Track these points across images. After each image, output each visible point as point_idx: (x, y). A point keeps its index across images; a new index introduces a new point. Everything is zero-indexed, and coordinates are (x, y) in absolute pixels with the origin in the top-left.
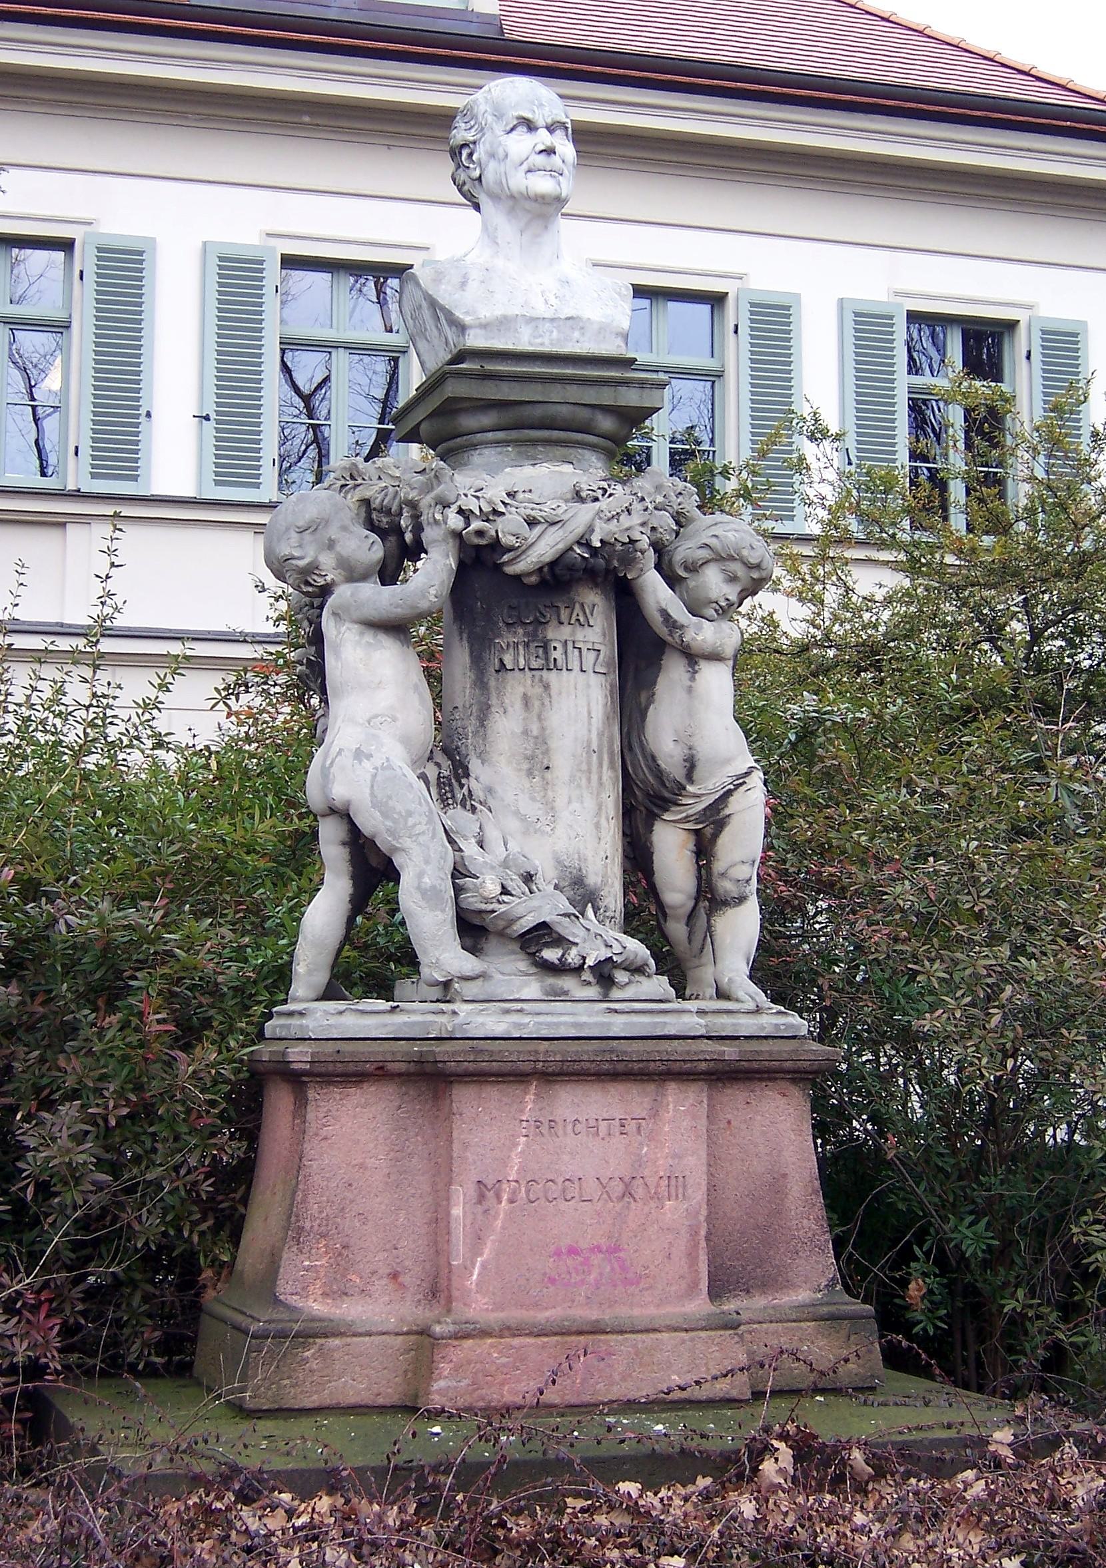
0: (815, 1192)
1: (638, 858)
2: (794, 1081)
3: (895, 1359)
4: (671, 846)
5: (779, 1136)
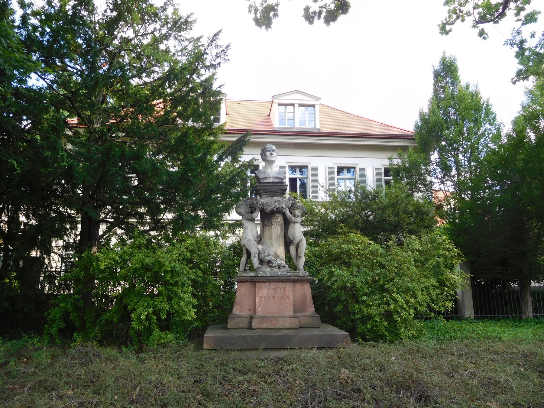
1: (287, 251)
3: (322, 322)
4: (292, 249)
5: (306, 290)
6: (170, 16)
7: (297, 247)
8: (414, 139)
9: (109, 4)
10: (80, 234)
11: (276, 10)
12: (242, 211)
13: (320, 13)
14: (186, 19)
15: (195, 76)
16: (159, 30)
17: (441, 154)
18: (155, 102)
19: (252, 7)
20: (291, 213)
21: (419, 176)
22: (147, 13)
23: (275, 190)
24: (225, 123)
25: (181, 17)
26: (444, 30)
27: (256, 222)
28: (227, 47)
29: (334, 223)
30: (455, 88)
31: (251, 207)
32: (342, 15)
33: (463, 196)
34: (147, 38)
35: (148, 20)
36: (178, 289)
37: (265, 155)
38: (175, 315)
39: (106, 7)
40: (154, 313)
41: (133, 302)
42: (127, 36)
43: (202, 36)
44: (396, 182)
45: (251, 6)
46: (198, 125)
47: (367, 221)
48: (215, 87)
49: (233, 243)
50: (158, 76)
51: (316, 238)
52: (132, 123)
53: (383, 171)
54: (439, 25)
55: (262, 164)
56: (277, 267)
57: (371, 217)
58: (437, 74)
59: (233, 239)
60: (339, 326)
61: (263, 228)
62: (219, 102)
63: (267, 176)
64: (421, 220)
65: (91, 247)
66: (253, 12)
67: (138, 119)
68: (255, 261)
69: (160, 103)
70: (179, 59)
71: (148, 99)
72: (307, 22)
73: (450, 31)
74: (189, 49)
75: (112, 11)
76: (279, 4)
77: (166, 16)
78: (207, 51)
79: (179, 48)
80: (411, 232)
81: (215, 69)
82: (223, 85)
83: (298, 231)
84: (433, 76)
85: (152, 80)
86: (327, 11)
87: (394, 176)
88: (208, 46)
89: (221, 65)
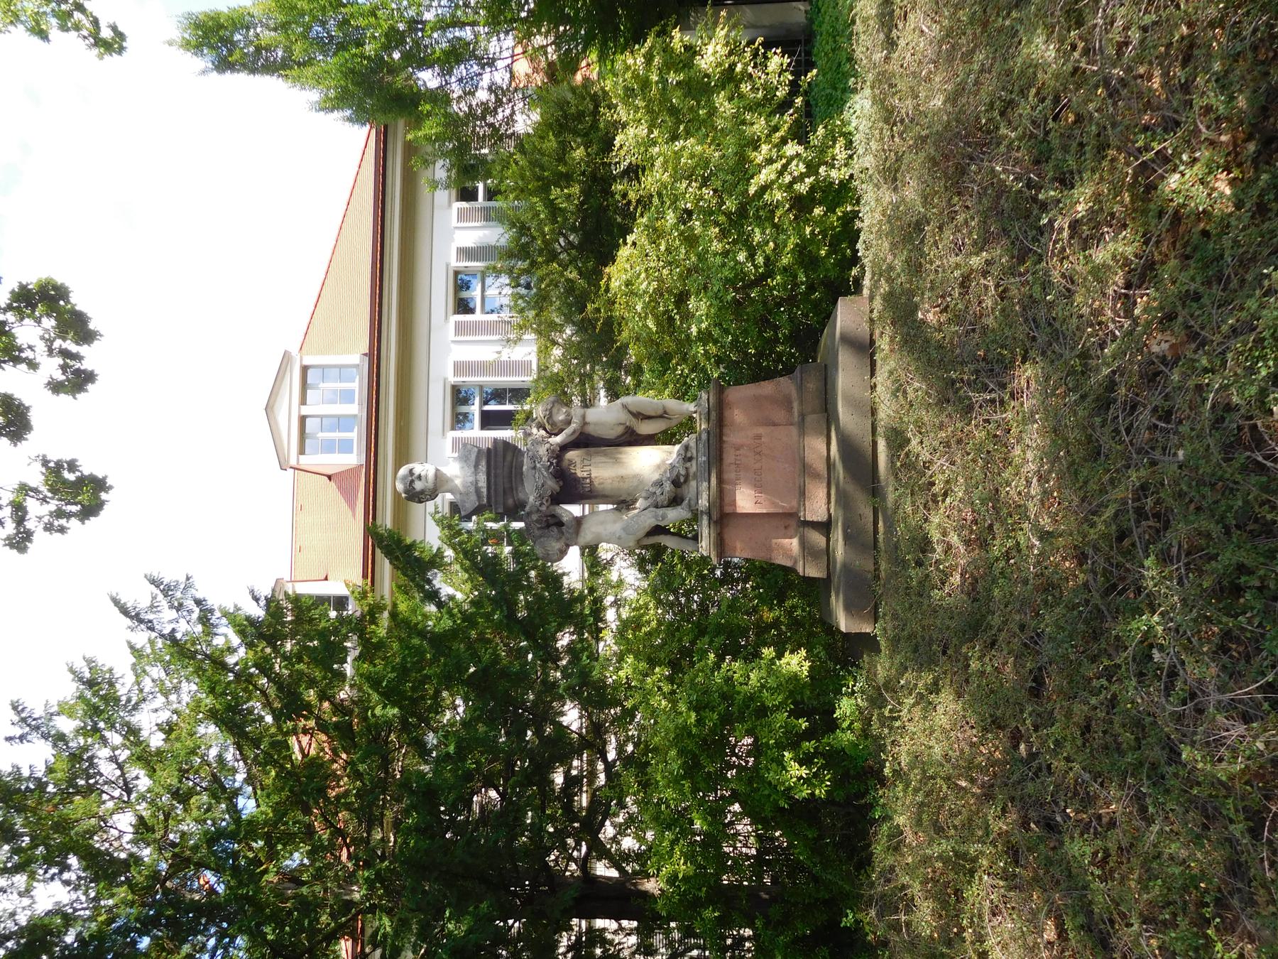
1: (650, 440)
4: (646, 428)
6: (77, 723)
8: (386, 127)
9: (48, 876)
10: (617, 919)
11: (59, 465)
12: (556, 545)
13: (65, 354)
14: (84, 683)
15: (231, 660)
16: (114, 749)
17: (424, 64)
18: (297, 756)
19: (52, 524)
20: (561, 431)
21: (476, 118)
22: (71, 782)
23: (506, 469)
24: (347, 585)
25: (81, 697)
26: (112, 44)
27: (587, 512)
28: (154, 582)
29: (584, 326)
30: (261, 22)
31: (548, 526)
32: (72, 300)
33: (523, 14)
34: (137, 778)
35: (89, 777)
36: (739, 693)
37: (422, 492)
38: (799, 698)
39: (57, 883)
40: (794, 746)
41: (769, 796)
42: (131, 830)
43: (129, 643)
44: (488, 175)
45: (49, 528)
46: (352, 646)
47: (580, 248)
48: (258, 612)
50: (231, 749)
51: (620, 368)
52: (347, 809)
53: (464, 204)
54: (101, 56)
56: (688, 464)
57: (571, 238)
58: (224, 65)
59: (624, 564)
61: (595, 497)
62: (296, 600)
63: (472, 489)
64: (578, 119)
65: (646, 895)
66: (63, 522)
67: (338, 797)
68: (674, 516)
69: (299, 742)
70: (186, 698)
71: (289, 776)
72: (90, 387)
73: (114, 28)
74: (163, 675)
75: (65, 867)
76: (44, 456)
77: (78, 732)
78: (166, 631)
79: (161, 700)
80: (608, 145)
81: (212, 611)
82: (252, 592)
83: (605, 413)
84: (228, 75)
85: (241, 763)
86: (60, 337)
87: (475, 178)
88: (152, 629)
89: (199, 596)
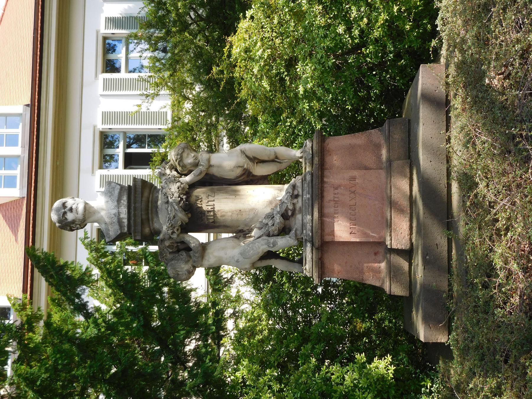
0: (354, 135)
2: (324, 142)
4: (260, 170)
7: (256, 160)
12: (185, 267)
20: (190, 172)
23: (144, 204)
29: (211, 85)
31: (178, 251)
37: (73, 222)
47: (207, 20)
49: (248, 283)
55: (91, 229)
56: (295, 201)
59: (242, 283)
60: (408, 82)
61: (218, 227)
63: (115, 220)
83: (227, 158)
